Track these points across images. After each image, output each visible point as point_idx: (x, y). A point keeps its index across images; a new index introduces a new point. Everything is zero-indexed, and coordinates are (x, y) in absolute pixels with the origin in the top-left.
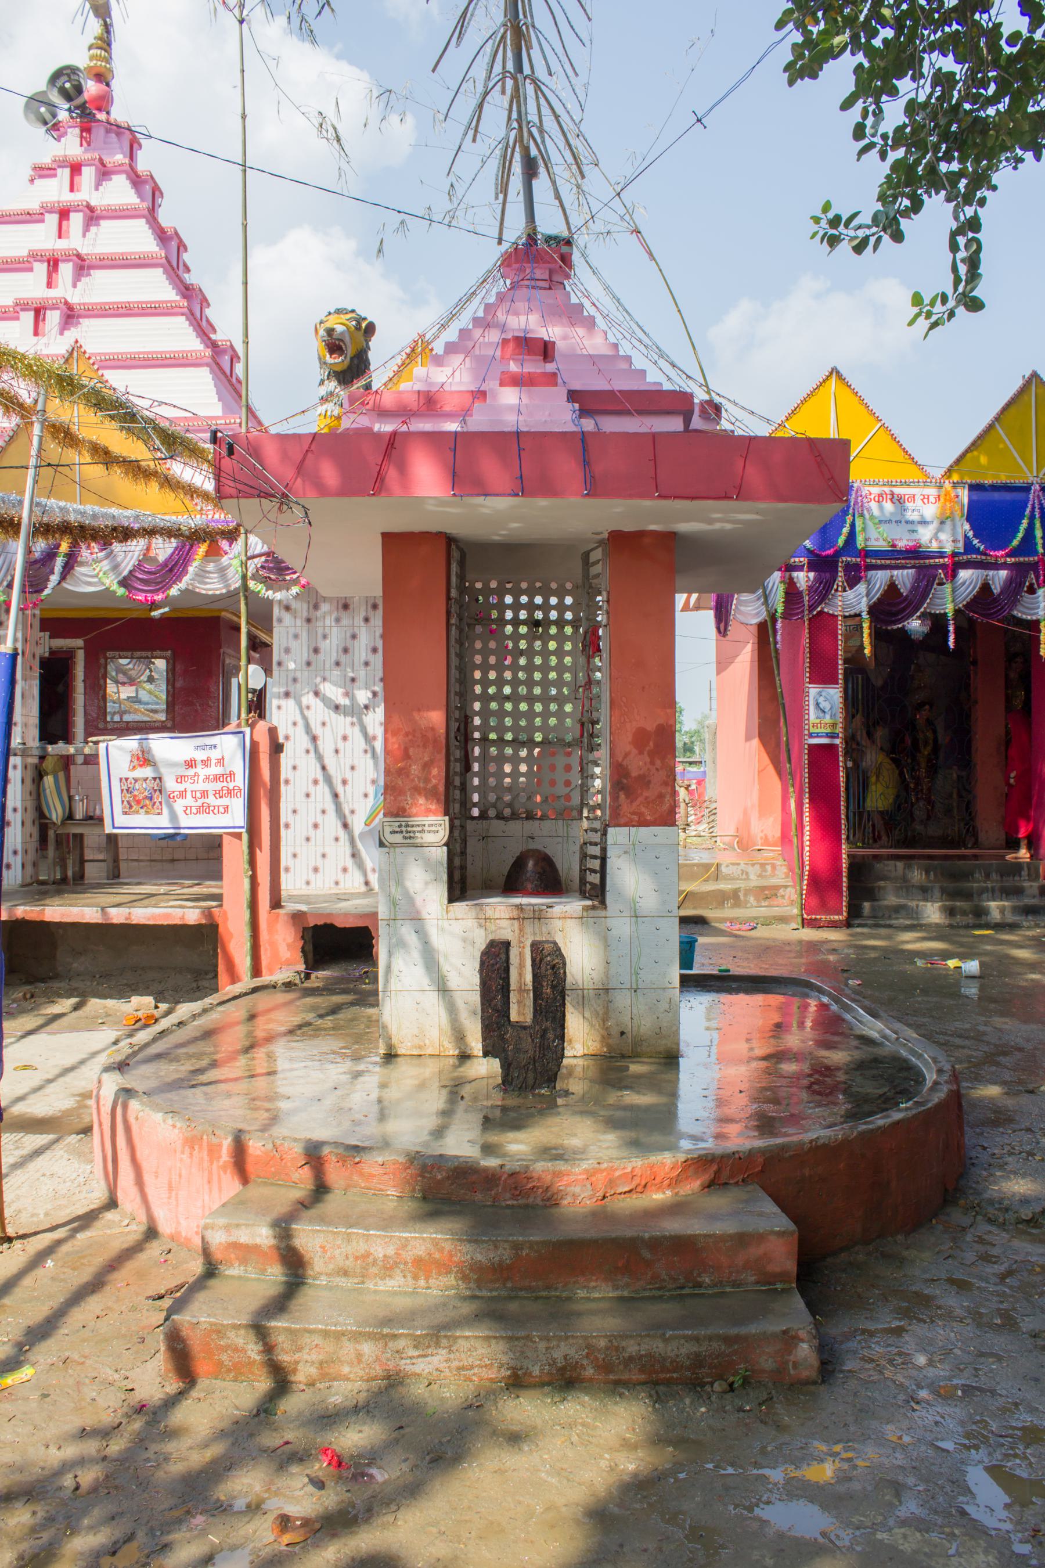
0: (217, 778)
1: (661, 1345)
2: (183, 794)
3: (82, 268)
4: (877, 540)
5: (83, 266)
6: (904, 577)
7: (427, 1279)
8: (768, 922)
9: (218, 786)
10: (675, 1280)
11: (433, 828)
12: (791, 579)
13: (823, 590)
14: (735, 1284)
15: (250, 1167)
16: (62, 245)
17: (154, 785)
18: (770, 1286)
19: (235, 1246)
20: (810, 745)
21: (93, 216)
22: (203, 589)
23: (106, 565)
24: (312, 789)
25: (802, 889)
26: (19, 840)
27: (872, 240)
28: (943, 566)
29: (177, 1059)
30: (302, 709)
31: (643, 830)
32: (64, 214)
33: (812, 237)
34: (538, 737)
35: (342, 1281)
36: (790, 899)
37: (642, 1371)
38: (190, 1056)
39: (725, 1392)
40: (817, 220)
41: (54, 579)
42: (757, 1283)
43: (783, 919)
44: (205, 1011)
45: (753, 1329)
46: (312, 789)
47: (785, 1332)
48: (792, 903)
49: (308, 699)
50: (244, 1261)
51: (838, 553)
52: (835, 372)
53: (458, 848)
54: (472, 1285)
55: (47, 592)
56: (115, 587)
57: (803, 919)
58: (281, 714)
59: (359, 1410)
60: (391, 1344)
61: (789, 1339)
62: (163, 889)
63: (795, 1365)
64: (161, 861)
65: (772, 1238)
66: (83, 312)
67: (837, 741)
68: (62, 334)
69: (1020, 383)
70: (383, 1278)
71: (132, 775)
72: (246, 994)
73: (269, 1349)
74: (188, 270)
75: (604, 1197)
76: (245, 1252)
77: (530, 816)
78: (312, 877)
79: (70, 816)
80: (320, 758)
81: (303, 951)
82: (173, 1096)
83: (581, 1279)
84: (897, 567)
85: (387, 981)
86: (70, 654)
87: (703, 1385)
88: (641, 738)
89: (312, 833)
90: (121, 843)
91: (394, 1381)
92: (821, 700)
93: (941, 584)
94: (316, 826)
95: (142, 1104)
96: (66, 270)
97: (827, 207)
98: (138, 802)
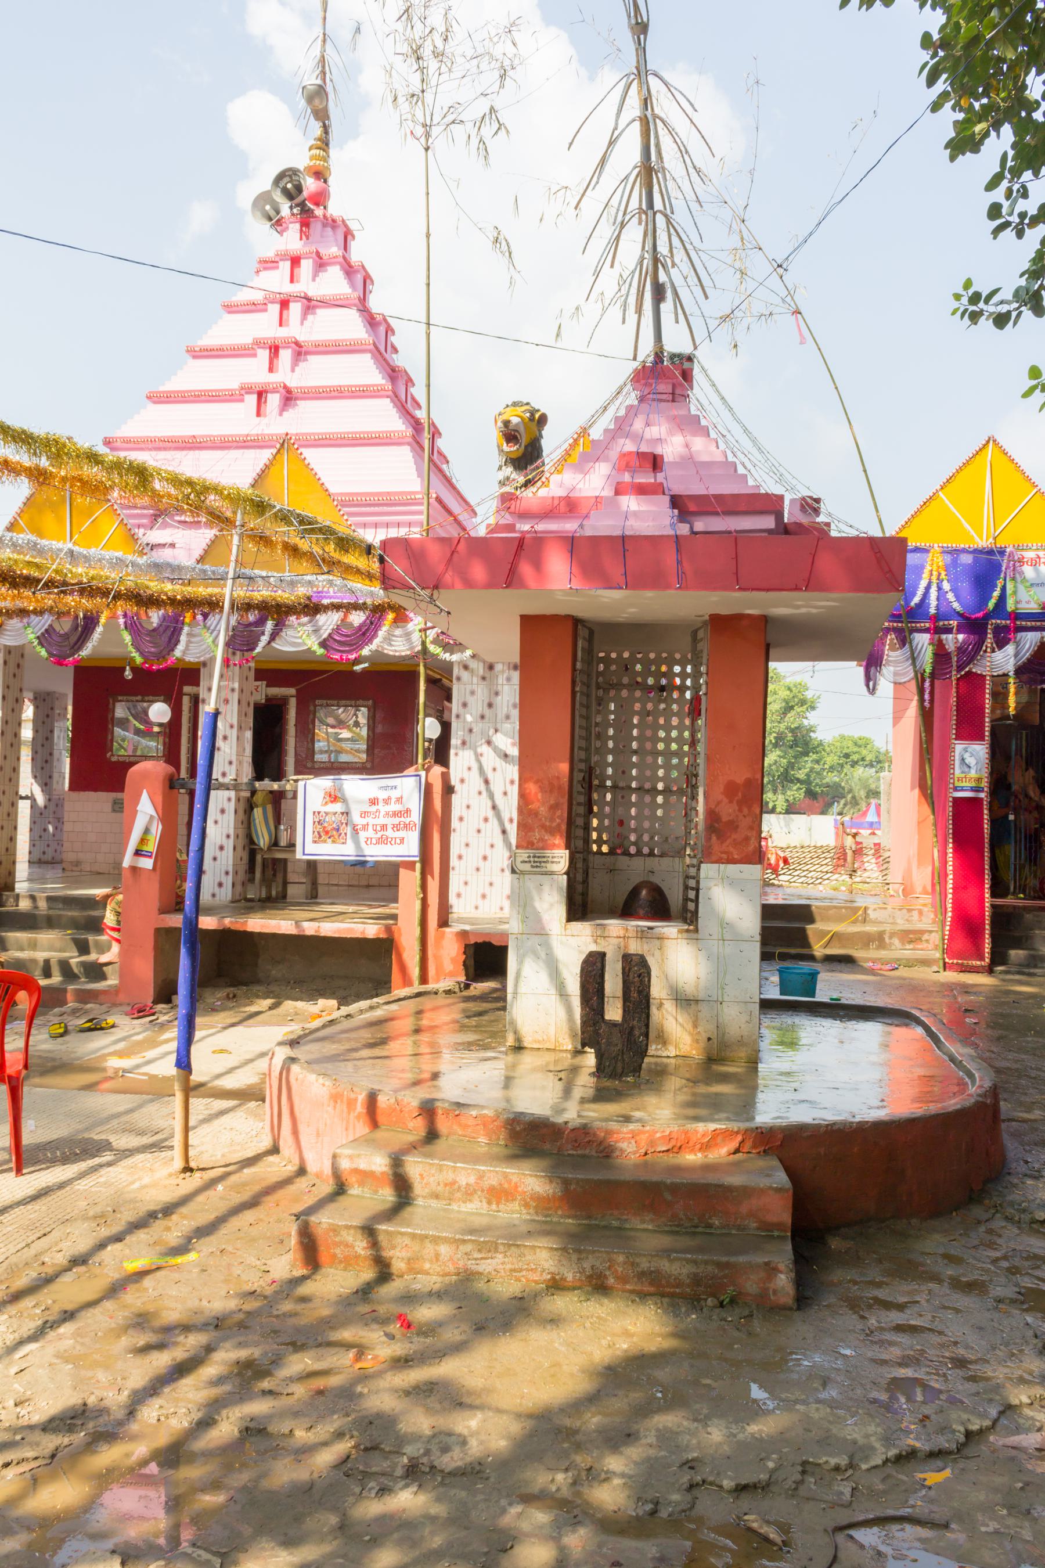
0: (395, 814)
1: (667, 1264)
2: (365, 827)
3: (299, 354)
4: (1028, 602)
5: (300, 352)
7: (498, 1204)
8: (910, 964)
9: (396, 821)
10: (691, 1220)
11: (560, 859)
12: (940, 641)
13: (970, 653)
14: (739, 1228)
15: (380, 1119)
16: (282, 333)
18: (768, 1231)
19: (356, 1171)
20: (956, 800)
21: (310, 305)
22: (389, 651)
23: (309, 628)
24: (482, 826)
25: (944, 935)
26: (231, 862)
27: (1014, 314)
29: (339, 1041)
30: (478, 757)
31: (731, 866)
32: (284, 304)
33: (953, 314)
34: (660, 786)
35: (434, 1203)
36: (934, 942)
37: (651, 1284)
38: (349, 1040)
39: (715, 1307)
40: (957, 297)
41: (264, 639)
42: (758, 1229)
43: (925, 962)
44: (371, 1008)
45: (741, 1259)
46: (482, 826)
47: (767, 1264)
48: (936, 948)
49: (484, 749)
50: (361, 1184)
51: (988, 616)
52: (991, 440)
53: (580, 877)
54: (532, 1211)
55: (258, 650)
57: (945, 963)
58: (460, 761)
59: (438, 1295)
60: (461, 1247)
61: (771, 1270)
62: (351, 909)
63: (775, 1292)
64: (358, 886)
65: (771, 1192)
67: (982, 795)
68: (281, 414)
70: (464, 1202)
71: (324, 809)
72: (410, 997)
73: (375, 1244)
74: (395, 350)
76: (365, 1176)
77: (651, 854)
78: (480, 902)
79: (275, 843)
80: (491, 796)
81: (465, 964)
82: (329, 1066)
83: (616, 1212)
85: (516, 985)
87: (699, 1300)
88: (731, 789)
89: (481, 864)
90: (320, 869)
91: (468, 1277)
92: (966, 756)
94: (485, 858)
95: (302, 1068)
96: (286, 356)
97: (968, 284)
98: (327, 833)
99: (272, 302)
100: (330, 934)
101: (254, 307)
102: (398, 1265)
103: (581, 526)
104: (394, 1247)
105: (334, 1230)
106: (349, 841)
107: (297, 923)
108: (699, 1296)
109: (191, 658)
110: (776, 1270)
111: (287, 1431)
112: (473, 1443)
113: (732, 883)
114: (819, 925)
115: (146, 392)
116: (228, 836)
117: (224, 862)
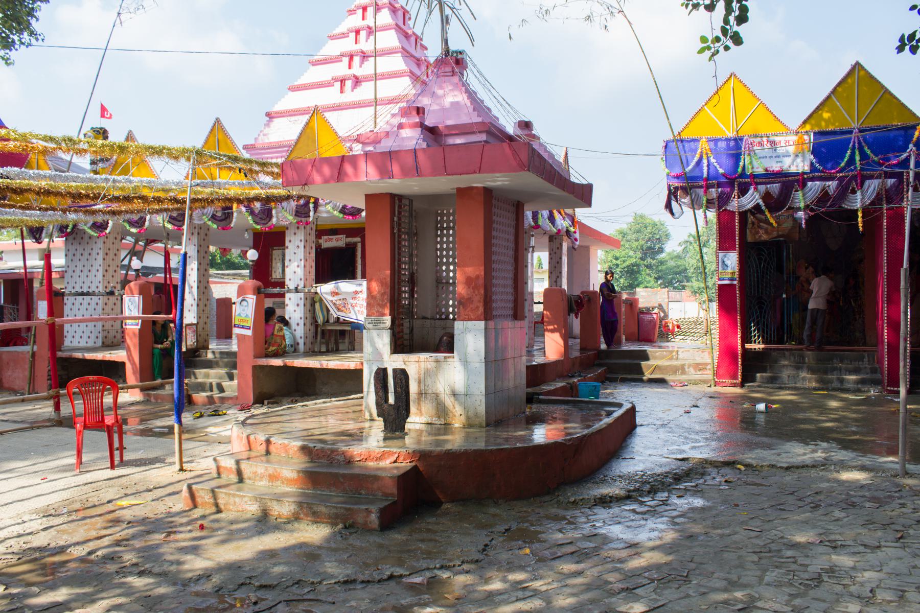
6: (775, 188)
11: (388, 320)
28: (797, 181)
32: (358, 32)
41: (312, 213)
61: (368, 512)
67: (735, 282)
69: (849, 67)
84: (769, 183)
86: (355, 244)
92: (725, 259)
93: (797, 191)
96: (357, 60)
100: (333, 367)
101: (344, 35)
108: (347, 525)
110: (371, 512)
114: (651, 362)
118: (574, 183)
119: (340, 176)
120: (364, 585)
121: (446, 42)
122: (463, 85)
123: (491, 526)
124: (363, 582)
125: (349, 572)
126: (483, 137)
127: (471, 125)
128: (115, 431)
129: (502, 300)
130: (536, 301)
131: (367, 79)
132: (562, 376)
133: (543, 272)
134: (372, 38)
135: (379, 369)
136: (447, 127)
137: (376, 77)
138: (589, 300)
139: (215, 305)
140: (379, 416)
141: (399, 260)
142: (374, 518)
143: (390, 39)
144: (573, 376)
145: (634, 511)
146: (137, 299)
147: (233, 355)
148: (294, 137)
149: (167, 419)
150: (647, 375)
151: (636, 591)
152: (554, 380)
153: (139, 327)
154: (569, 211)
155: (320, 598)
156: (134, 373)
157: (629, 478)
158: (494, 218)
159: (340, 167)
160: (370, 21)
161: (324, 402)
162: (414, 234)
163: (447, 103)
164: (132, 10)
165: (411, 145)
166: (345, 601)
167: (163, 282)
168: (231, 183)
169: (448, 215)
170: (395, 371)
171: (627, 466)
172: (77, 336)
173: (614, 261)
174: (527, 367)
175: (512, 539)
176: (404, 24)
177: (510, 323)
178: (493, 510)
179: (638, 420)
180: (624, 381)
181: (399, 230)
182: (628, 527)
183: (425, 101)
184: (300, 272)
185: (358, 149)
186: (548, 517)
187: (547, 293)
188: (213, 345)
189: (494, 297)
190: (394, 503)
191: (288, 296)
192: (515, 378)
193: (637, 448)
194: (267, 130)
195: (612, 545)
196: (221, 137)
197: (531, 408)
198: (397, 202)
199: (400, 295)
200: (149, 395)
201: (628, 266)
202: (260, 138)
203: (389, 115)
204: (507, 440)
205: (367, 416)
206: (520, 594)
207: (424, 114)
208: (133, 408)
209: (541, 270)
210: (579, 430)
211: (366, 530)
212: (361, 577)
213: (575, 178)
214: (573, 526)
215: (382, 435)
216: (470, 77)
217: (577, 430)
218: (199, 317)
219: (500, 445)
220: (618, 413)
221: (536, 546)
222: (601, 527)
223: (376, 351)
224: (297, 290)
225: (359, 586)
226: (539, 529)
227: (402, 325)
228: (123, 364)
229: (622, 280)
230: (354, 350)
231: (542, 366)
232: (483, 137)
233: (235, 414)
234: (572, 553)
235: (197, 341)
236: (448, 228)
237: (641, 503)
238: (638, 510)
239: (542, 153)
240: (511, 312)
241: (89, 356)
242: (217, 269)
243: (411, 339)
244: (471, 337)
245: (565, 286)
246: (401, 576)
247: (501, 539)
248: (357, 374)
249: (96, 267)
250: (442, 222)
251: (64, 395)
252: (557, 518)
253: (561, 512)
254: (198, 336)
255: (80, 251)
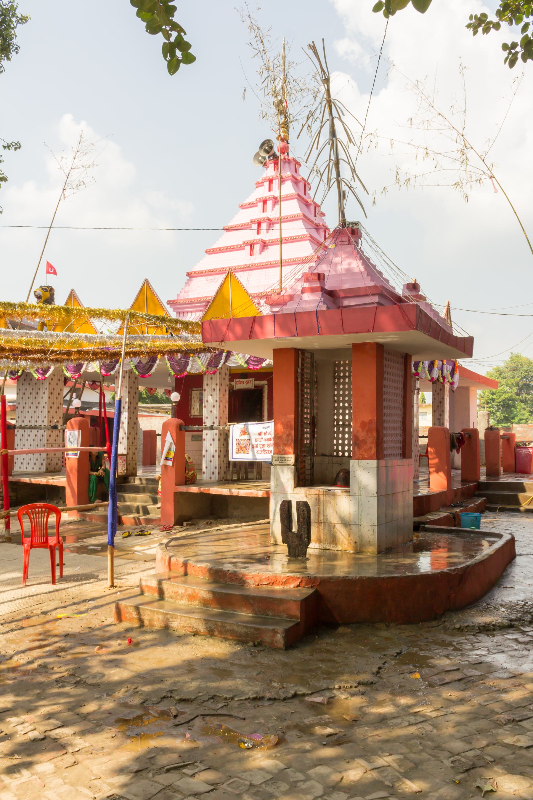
2: (257, 446)
3: (270, 224)
11: (291, 458)
15: (172, 568)
17: (248, 442)
19: (147, 586)
26: (217, 463)
32: (265, 202)
41: (222, 361)
42: (287, 617)
47: (273, 630)
50: (149, 592)
56: (243, 364)
61: (275, 632)
63: (276, 642)
65: (292, 602)
66: (269, 243)
68: (260, 253)
73: (139, 613)
75: (258, 585)
76: (150, 587)
86: (262, 387)
98: (241, 449)
99: (259, 202)
101: (253, 205)
102: (146, 622)
103: (282, 309)
104: (145, 615)
105: (126, 607)
106: (250, 452)
107: (230, 489)
109: (194, 372)
111: (52, 667)
112: (106, 677)
113: (365, 468)
115: (205, 250)
116: (216, 451)
117: (214, 463)
118: (456, 337)
119: (251, 335)
120: (271, 702)
121: (342, 213)
122: (358, 253)
123: (384, 649)
124: (270, 699)
125: (257, 689)
126: (376, 299)
127: (366, 288)
128: (56, 551)
129: (390, 439)
130: (420, 435)
131: (273, 243)
132: (446, 506)
133: (426, 406)
134: (277, 207)
135: (284, 501)
136: (344, 291)
137: (281, 241)
138: (470, 437)
139: (142, 434)
140: (283, 542)
141: (302, 405)
142: (279, 638)
143: (292, 208)
144: (455, 506)
145: (516, 640)
146: (76, 433)
147: (155, 481)
148: (213, 294)
149: (100, 537)
150: (524, 506)
151: (523, 723)
152: (438, 510)
153: (78, 457)
154: (454, 360)
155: (232, 713)
156: (73, 496)
157: (511, 607)
158: (386, 369)
159: (251, 327)
160: (275, 193)
161: (236, 527)
162: (315, 383)
163: (343, 268)
164: (74, 186)
165: (311, 307)
166: (255, 717)
167: (98, 415)
168: (155, 338)
169: (345, 365)
170: (298, 503)
171: (509, 595)
172: (25, 463)
173: (491, 396)
174: (415, 498)
175: (402, 663)
176: (305, 194)
177: (398, 461)
178: (384, 634)
179: (518, 550)
180: (502, 510)
181: (302, 380)
182: (511, 656)
183: (323, 268)
184: (216, 411)
185: (266, 310)
186: (435, 643)
187: (431, 431)
188: (140, 472)
189: (385, 439)
190: (298, 624)
191: (205, 432)
192: (404, 508)
193: (517, 578)
194: (187, 289)
195: (497, 675)
196: (149, 295)
197: (418, 536)
198: (300, 355)
199: (302, 436)
200: (84, 516)
201: (504, 400)
202: (182, 295)
203: (294, 280)
204: (397, 567)
205: (272, 542)
206: (412, 719)
207: (324, 279)
208: (71, 527)
209: (424, 405)
210: (462, 560)
211: (273, 648)
212: (268, 695)
213: (458, 332)
214: (459, 653)
215: (287, 559)
216: (364, 245)
217: (462, 561)
218: (129, 449)
219: (391, 572)
220: (499, 543)
221: (426, 671)
222: (485, 655)
223: (284, 486)
224: (212, 428)
225: (267, 703)
226: (428, 654)
227: (304, 462)
228: (63, 488)
229: (498, 414)
230: (261, 479)
231: (427, 498)
232: (376, 299)
233: (158, 536)
234: (459, 680)
235: (127, 469)
236: (344, 377)
237: (523, 633)
238: (520, 640)
239: (428, 312)
240: (400, 452)
241: (35, 480)
242: (143, 403)
243: (312, 474)
244: (365, 474)
245: (447, 425)
246: (304, 695)
247: (393, 662)
248: (264, 502)
249: (42, 404)
250: (339, 371)
251: (14, 516)
252: (445, 644)
253: (448, 638)
254: (128, 464)
255: (29, 390)
